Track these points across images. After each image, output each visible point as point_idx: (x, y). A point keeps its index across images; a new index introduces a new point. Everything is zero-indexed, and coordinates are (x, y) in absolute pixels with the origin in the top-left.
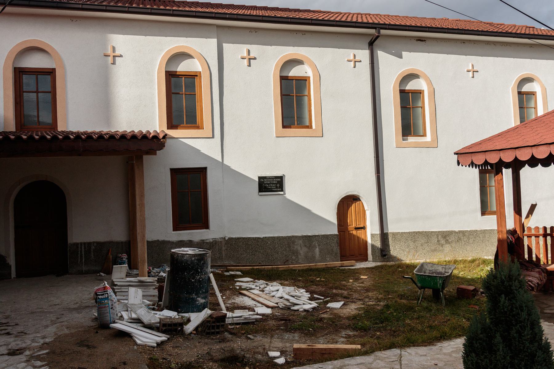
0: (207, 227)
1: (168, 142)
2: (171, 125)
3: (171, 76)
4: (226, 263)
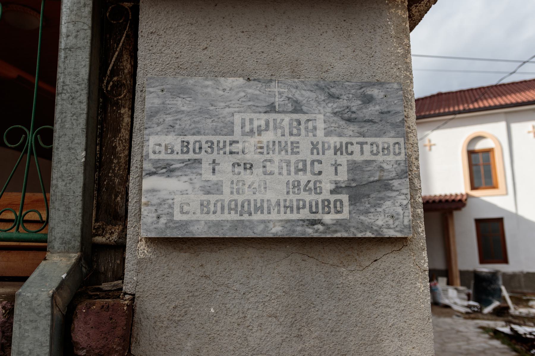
0: (505, 261)
1: (469, 203)
2: (473, 187)
3: (471, 153)
4: (525, 291)
